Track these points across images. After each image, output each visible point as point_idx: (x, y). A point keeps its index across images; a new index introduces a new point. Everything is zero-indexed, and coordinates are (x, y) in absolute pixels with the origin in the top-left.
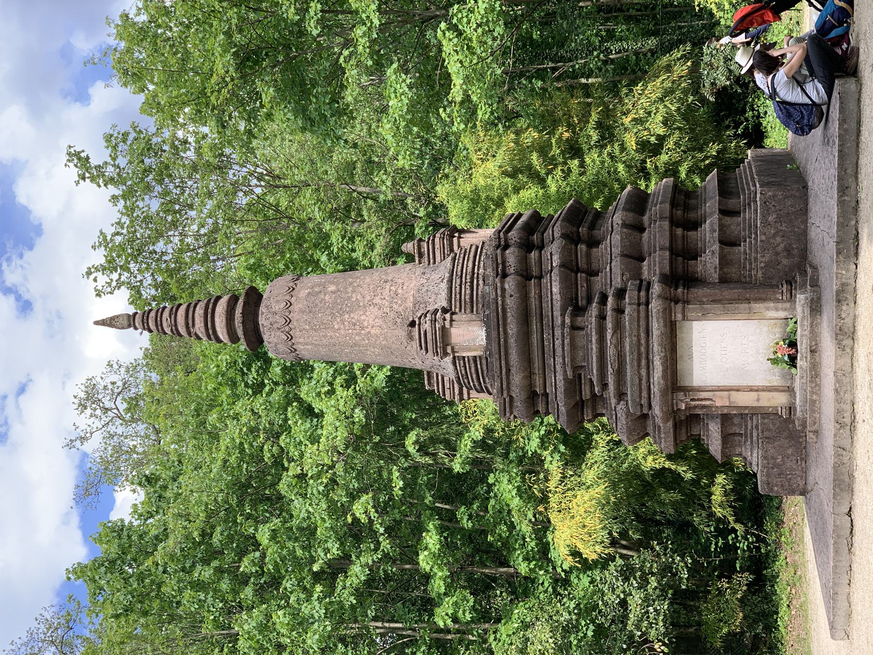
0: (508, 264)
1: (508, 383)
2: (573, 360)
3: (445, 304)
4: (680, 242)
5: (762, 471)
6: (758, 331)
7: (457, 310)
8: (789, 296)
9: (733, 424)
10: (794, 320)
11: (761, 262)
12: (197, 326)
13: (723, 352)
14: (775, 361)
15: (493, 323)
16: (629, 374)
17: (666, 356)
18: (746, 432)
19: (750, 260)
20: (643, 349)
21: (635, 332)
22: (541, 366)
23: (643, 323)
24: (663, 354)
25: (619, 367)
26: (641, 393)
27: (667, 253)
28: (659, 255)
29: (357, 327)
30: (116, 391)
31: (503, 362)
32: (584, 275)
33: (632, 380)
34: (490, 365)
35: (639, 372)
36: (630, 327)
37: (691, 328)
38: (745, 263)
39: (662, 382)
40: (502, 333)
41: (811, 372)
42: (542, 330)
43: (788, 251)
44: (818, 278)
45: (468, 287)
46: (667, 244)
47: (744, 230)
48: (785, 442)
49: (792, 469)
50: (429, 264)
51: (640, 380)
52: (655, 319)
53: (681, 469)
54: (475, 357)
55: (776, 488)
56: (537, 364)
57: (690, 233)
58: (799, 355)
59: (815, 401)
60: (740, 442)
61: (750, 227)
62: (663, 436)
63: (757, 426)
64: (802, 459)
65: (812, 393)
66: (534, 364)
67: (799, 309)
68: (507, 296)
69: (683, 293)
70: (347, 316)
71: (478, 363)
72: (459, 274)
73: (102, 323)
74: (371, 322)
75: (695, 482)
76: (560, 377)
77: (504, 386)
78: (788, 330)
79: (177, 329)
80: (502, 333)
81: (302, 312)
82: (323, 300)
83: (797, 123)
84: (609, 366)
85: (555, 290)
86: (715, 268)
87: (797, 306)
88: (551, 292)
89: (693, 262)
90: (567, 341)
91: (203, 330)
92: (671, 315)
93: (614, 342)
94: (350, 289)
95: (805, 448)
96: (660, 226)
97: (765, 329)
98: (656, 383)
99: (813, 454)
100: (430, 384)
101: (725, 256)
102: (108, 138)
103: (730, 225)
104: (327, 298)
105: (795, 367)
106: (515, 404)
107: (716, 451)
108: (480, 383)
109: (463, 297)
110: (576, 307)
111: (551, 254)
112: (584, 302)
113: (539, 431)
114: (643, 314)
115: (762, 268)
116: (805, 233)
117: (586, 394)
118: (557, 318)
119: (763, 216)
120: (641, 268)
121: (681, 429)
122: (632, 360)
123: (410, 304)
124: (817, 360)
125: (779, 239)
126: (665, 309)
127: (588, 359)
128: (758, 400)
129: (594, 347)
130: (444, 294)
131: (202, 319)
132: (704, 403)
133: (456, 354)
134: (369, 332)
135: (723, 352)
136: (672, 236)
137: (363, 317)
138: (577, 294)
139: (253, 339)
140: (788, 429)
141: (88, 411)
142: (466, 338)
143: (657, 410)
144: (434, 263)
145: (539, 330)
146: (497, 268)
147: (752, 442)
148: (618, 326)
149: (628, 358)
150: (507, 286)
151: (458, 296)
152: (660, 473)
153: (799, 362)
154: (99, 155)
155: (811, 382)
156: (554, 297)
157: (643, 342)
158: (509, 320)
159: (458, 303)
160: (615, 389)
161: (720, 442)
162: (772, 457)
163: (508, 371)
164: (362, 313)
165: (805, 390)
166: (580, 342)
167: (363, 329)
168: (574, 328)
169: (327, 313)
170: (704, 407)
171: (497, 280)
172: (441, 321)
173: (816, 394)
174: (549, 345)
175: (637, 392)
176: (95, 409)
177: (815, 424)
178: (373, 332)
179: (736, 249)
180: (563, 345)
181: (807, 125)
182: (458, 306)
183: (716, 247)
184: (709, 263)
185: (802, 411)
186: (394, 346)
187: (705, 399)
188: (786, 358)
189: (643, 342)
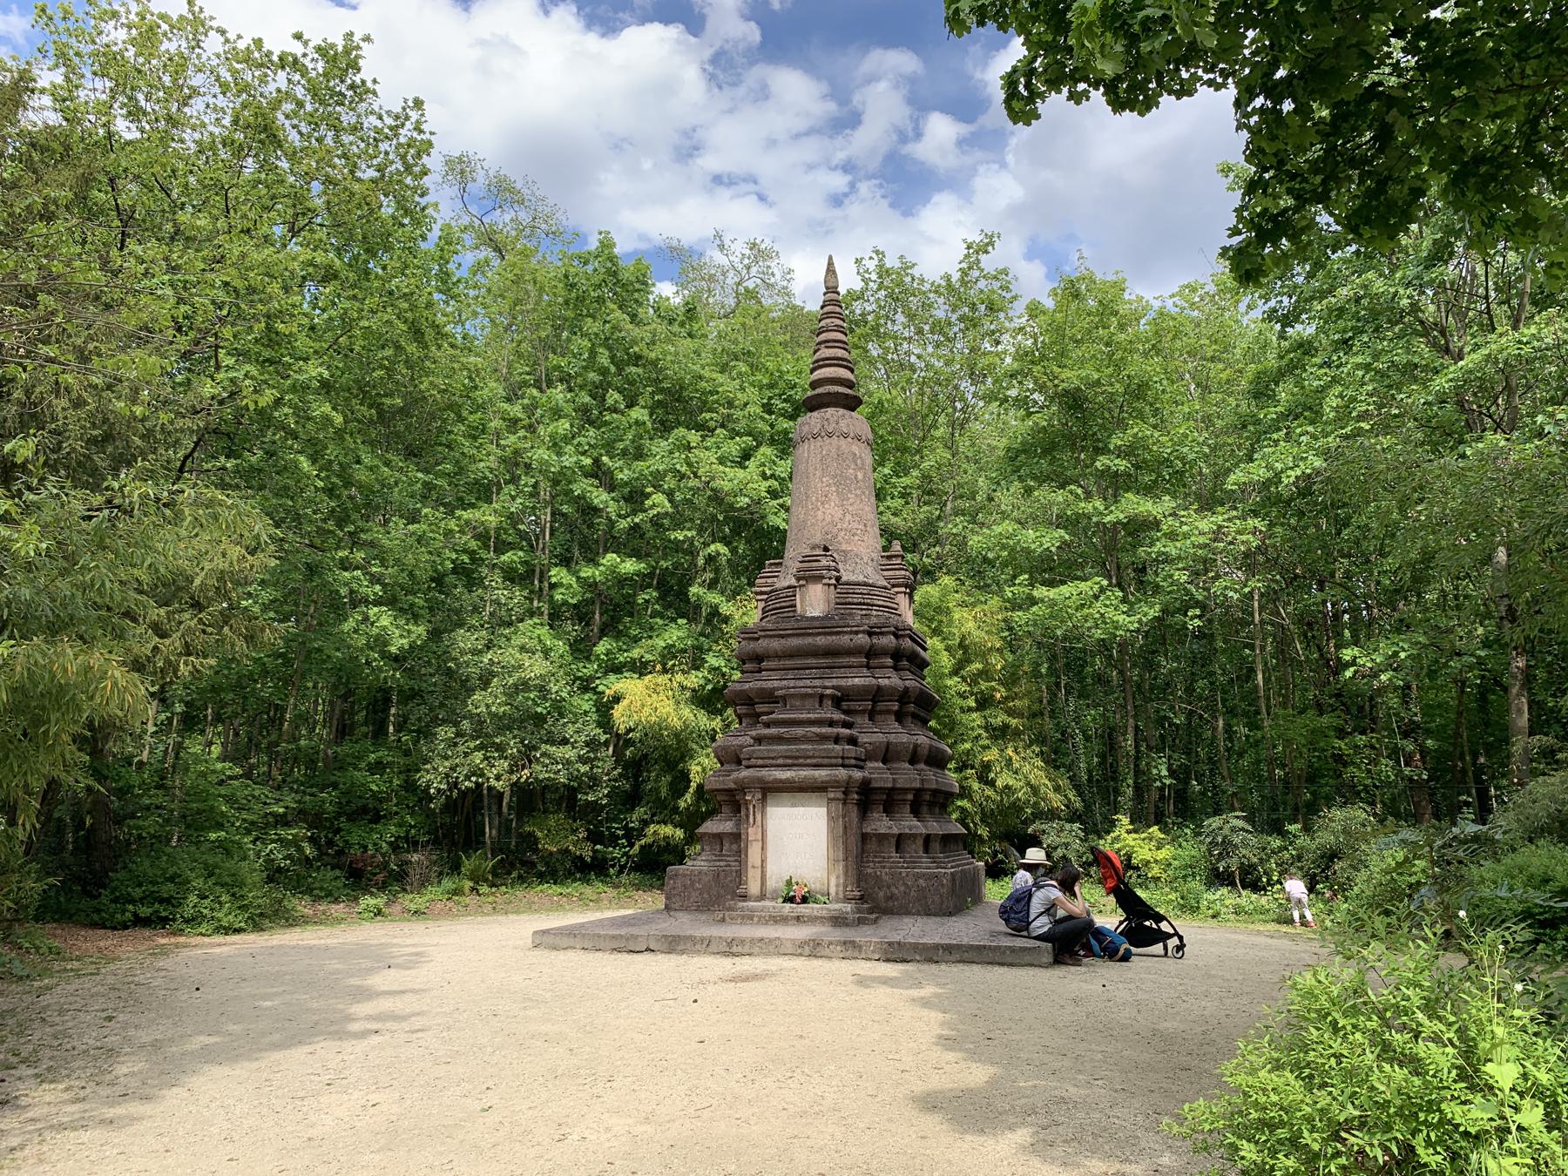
2: (792, 696)
3: (844, 579)
14: (789, 883)
23: (826, 761)
43: (891, 897)
53: (688, 797)
56: (789, 663)
67: (837, 906)
73: (830, 263)
75: (676, 809)
99: (704, 917)
110: (839, 699)
114: (834, 761)
116: (908, 913)
117: (760, 708)
130: (853, 578)
136: (905, 790)
141: (748, 252)
143: (745, 773)
148: (823, 738)
152: (685, 778)
153: (788, 905)
163: (782, 636)
166: (808, 703)
168: (822, 697)
183: (896, 831)
184: (881, 824)
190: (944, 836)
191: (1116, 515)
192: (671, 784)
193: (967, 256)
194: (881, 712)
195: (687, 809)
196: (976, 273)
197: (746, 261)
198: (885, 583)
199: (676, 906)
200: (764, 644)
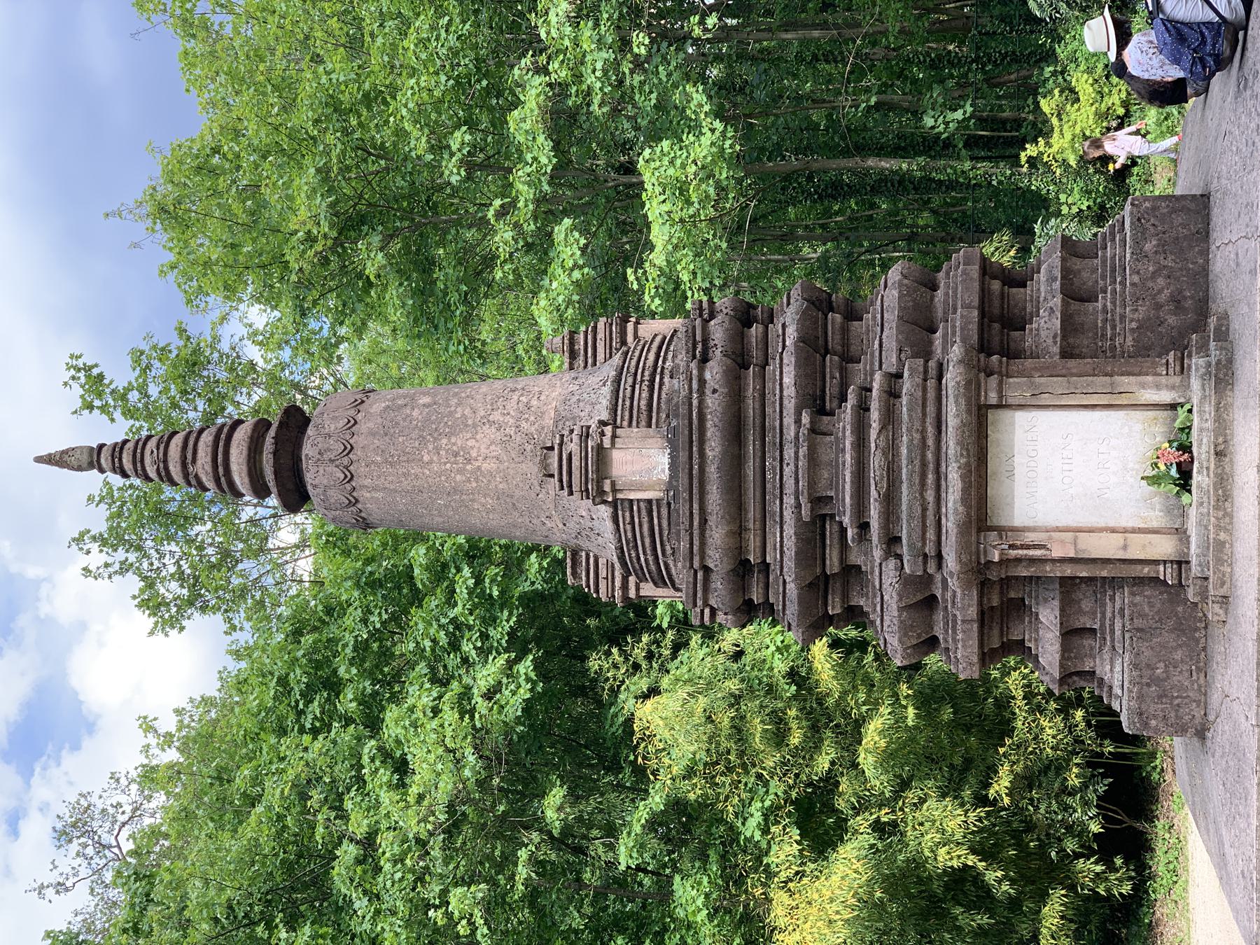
0: (712, 343)
1: (703, 544)
2: (812, 484)
3: (605, 416)
4: (996, 303)
5: (1130, 691)
6: (1126, 429)
7: (625, 423)
8: (1178, 368)
9: (1081, 612)
10: (1187, 407)
11: (1132, 321)
12: (199, 462)
13: (1066, 467)
14: (1154, 480)
15: (682, 439)
16: (905, 499)
17: (968, 464)
18: (1103, 625)
19: (1113, 320)
20: (930, 456)
21: (917, 425)
22: (758, 516)
23: (931, 409)
24: (963, 461)
25: (888, 489)
26: (924, 533)
27: (976, 313)
28: (962, 316)
29: (460, 459)
30: (122, 818)
31: (696, 506)
32: (836, 358)
33: (910, 508)
34: (674, 515)
35: (921, 495)
36: (910, 416)
37: (1013, 424)
38: (1104, 328)
39: (961, 509)
40: (696, 455)
41: (1216, 490)
42: (764, 453)
43: (1177, 300)
44: (1228, 329)
45: (645, 387)
46: (976, 303)
47: (1104, 277)
48: (1168, 638)
49: (1182, 688)
50: (585, 367)
51: (924, 510)
52: (951, 399)
53: (992, 876)
54: (649, 502)
55: (1153, 723)
56: (752, 512)
57: (1014, 290)
58: (1196, 465)
59: (1224, 543)
60: (1092, 649)
61: (1113, 270)
62: (960, 636)
63: (1122, 610)
64: (1199, 670)
65: (1219, 528)
66: (747, 512)
67: (1195, 383)
68: (708, 392)
69: (1001, 362)
70: (444, 441)
71: (655, 514)
72: (632, 370)
73: (49, 460)
74: (483, 450)
75: (1014, 904)
76: (789, 530)
77: (696, 548)
78: (1177, 424)
79: (166, 469)
80: (696, 455)
81: (373, 434)
82: (408, 416)
83: (1195, 51)
84: (873, 487)
85: (788, 380)
86: (1055, 337)
87: (1192, 380)
88: (781, 384)
89: (1017, 334)
90: (803, 451)
91: (209, 468)
92: (979, 395)
93: (882, 444)
94: (454, 401)
95: (1204, 649)
96: (964, 272)
97: (1139, 427)
98: (951, 511)
99: (1217, 648)
100: (574, 574)
101: (1071, 316)
102: (137, 355)
103: (1079, 271)
104: (415, 413)
105: (1189, 491)
106: (713, 586)
107: (1050, 664)
108: (657, 558)
109: (635, 403)
110: (818, 403)
111: (784, 326)
112: (835, 404)
113: (763, 802)
114: (931, 394)
115: (1132, 330)
116: (1205, 271)
117: (833, 564)
118: (788, 429)
119: (1136, 242)
120: (931, 343)
121: (991, 628)
122: (911, 475)
123: (549, 422)
124: (1227, 469)
125: (1161, 281)
126: (968, 383)
127: (837, 483)
128: (1125, 547)
129: (848, 457)
130: (605, 402)
131: (209, 449)
132: (1031, 553)
133: (620, 496)
134: (479, 468)
135: (1066, 467)
136: (984, 293)
137: (471, 443)
138: (823, 391)
139: (290, 486)
140: (1176, 615)
141: (74, 847)
142: (637, 467)
143: (951, 561)
144: (594, 364)
145: (759, 454)
146: (695, 348)
147: (1113, 640)
148: (890, 418)
149: (904, 471)
150: (708, 376)
151: (628, 403)
152: (961, 879)
153: (1196, 478)
154: (120, 375)
155: (1217, 508)
156: (785, 393)
157: (930, 442)
158: (709, 434)
159: (627, 413)
160: (880, 528)
161: (1057, 647)
162: (1148, 666)
163: (704, 521)
164: (469, 435)
165: (1206, 528)
166: (826, 455)
167: (469, 461)
168: (813, 430)
169: (413, 436)
170: (1032, 561)
171: (693, 365)
172: (597, 437)
173: (1226, 530)
174: (774, 478)
175: (919, 531)
176: (85, 846)
177: (1223, 584)
178: (485, 466)
179: (1090, 306)
180: (797, 458)
181: (1210, 55)
182: (627, 418)
183: (1057, 301)
184: (1046, 325)
185: (1200, 565)
186: (518, 493)
187: (1035, 547)
188: (1174, 472)
189: (930, 442)
190: (1061, 578)
191: (543, 153)
192: (968, 908)
193: (104, 409)
194: (846, 343)
195: (1013, 882)
196: (134, 396)
197: (90, 851)
198: (617, 359)
199: (1198, 713)
200: (716, 559)
